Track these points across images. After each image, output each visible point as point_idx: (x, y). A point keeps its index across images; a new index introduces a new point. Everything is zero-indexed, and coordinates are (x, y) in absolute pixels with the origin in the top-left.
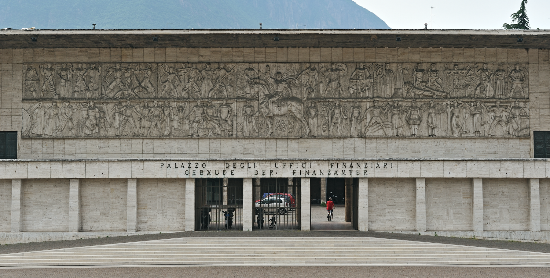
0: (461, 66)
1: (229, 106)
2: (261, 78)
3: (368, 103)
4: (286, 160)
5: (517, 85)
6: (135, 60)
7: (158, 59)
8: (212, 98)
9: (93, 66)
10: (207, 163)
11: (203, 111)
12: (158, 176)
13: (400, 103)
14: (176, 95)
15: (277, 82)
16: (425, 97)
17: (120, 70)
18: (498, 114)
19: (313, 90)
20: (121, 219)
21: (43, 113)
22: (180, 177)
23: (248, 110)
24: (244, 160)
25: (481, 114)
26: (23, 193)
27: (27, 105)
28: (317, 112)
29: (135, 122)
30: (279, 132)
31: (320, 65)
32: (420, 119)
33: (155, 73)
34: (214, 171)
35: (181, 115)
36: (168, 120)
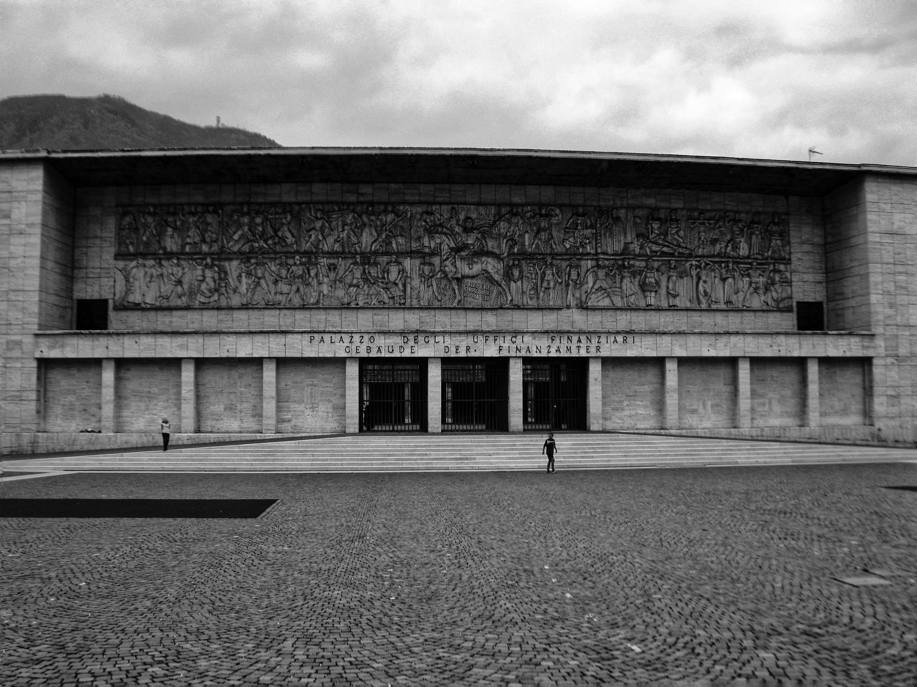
0: (708, 215)
1: (400, 263)
2: (445, 224)
3: (589, 262)
4: (489, 332)
5: (777, 242)
6: (271, 199)
7: (301, 199)
8: (376, 253)
9: (211, 209)
10: (376, 336)
11: (364, 270)
12: (307, 354)
13: (632, 262)
14: (326, 249)
15: (467, 230)
16: (664, 254)
17: (248, 214)
18: (755, 280)
19: (516, 243)
20: (254, 416)
21: (142, 274)
22: (338, 355)
23: (427, 269)
24: (430, 332)
25: (734, 278)
26: (118, 379)
27: (121, 264)
28: (521, 272)
29: (268, 285)
30: (470, 299)
31: (525, 209)
32: (658, 283)
33: (297, 217)
34: (388, 347)
35: (332, 275)
36: (315, 282)
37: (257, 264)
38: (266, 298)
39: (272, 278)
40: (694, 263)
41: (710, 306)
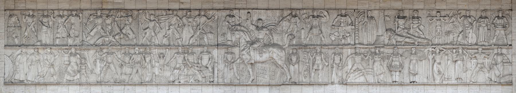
0: (443, 13)
1: (210, 53)
3: (349, 50)
5: (500, 32)
7: (139, 7)
8: (192, 45)
9: (74, 13)
14: (157, 42)
17: (101, 17)
21: (25, 59)
23: (229, 57)
27: (9, 51)
29: (116, 69)
31: (302, 12)
32: (401, 66)
35: (162, 61)
36: (149, 66)
37: (108, 53)
38: (115, 77)
39: (119, 63)
40: (431, 49)
41: (442, 82)
